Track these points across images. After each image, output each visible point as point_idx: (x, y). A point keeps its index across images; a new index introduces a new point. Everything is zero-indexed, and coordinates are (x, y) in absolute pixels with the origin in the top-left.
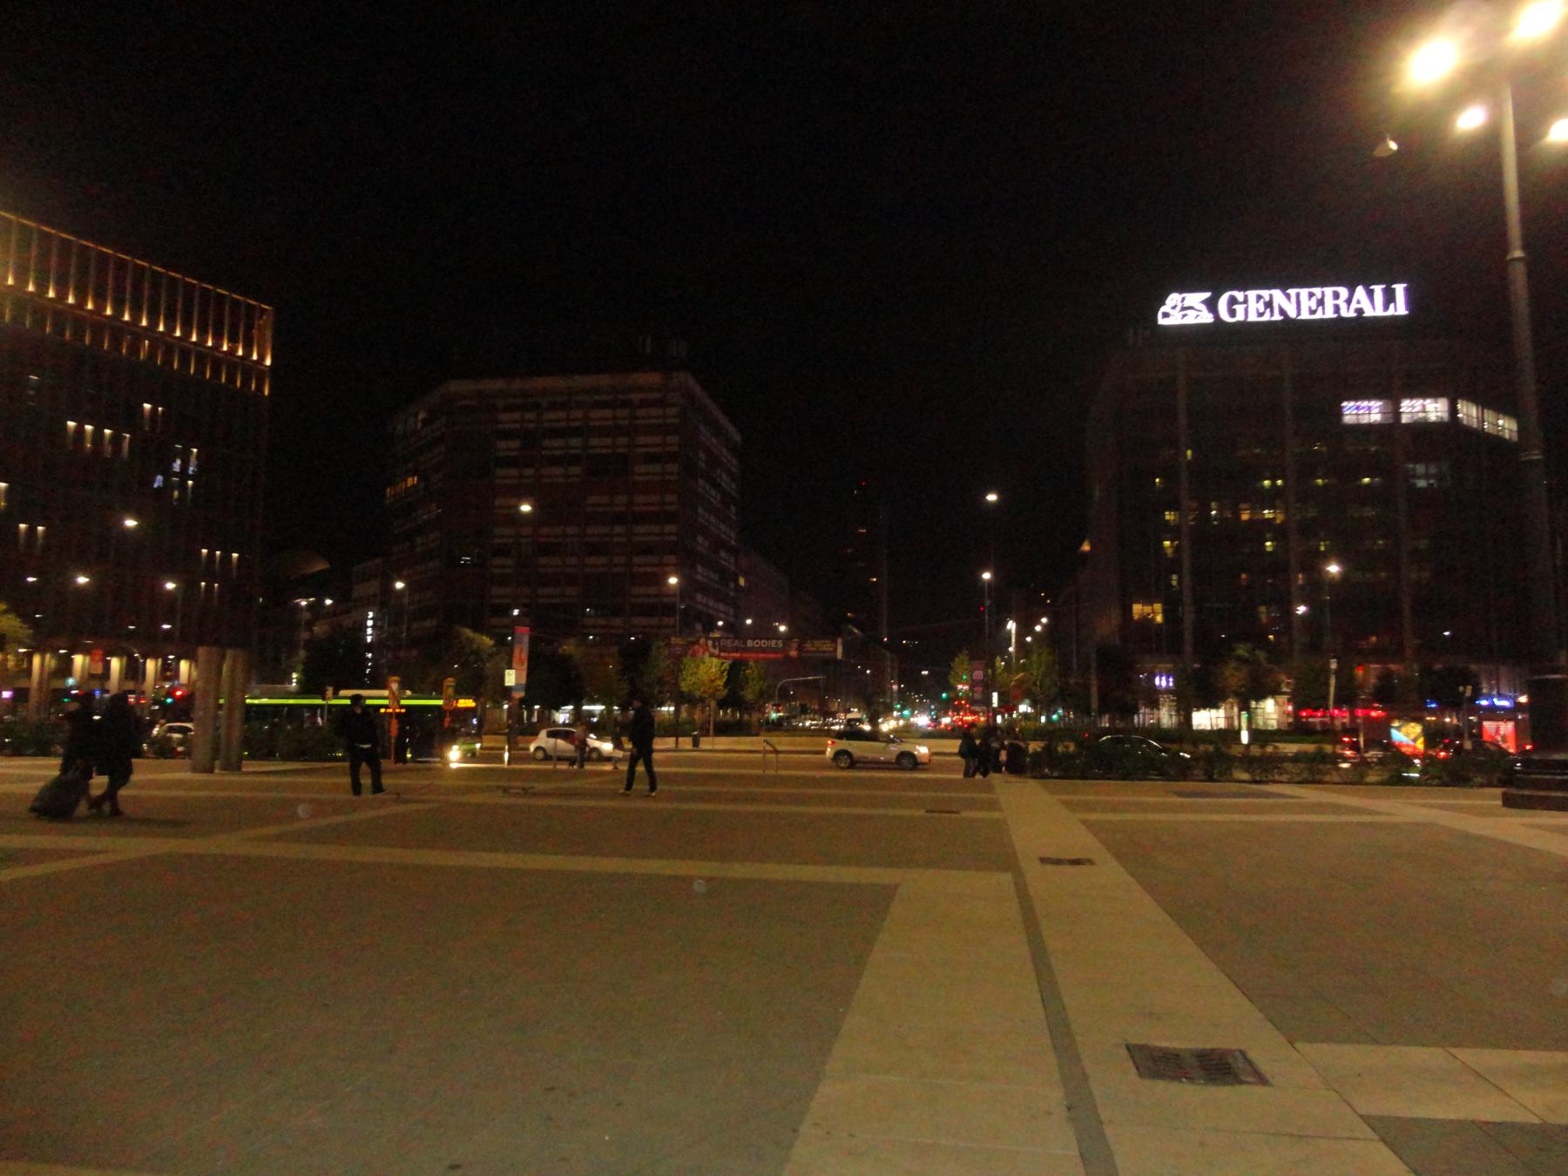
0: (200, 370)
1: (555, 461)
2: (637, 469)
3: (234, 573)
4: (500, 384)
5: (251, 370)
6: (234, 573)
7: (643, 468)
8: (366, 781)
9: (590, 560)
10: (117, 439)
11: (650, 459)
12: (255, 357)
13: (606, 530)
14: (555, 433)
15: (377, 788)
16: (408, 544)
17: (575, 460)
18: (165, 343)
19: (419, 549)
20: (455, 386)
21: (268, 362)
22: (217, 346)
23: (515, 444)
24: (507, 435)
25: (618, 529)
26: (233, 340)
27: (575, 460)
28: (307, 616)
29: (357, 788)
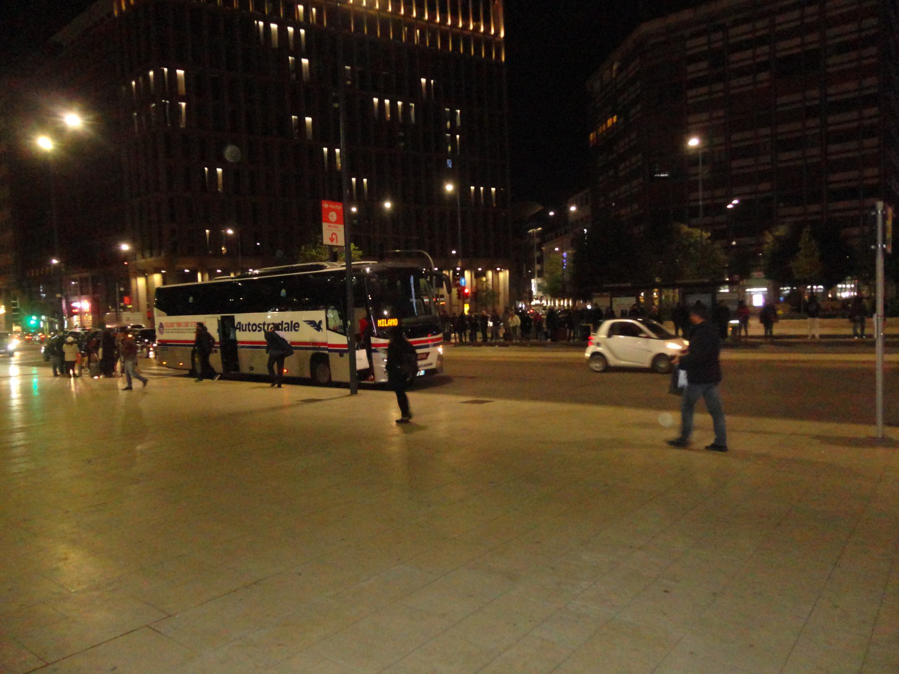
0: (467, 49)
1: (741, 73)
2: (830, 61)
3: (310, 136)
4: (686, 15)
5: (489, 41)
6: (310, 136)
7: (834, 59)
8: (702, 437)
9: (783, 156)
10: (406, 107)
11: (841, 49)
12: (493, 32)
13: (799, 126)
14: (738, 47)
15: (719, 446)
16: (864, 300)
17: (763, 67)
18: (429, 28)
19: (621, 174)
20: (646, 28)
21: (502, 34)
22: (466, 26)
23: (704, 65)
24: (694, 59)
25: (810, 123)
26: (476, 20)
27: (763, 67)
28: (537, 240)
29: (56, 375)
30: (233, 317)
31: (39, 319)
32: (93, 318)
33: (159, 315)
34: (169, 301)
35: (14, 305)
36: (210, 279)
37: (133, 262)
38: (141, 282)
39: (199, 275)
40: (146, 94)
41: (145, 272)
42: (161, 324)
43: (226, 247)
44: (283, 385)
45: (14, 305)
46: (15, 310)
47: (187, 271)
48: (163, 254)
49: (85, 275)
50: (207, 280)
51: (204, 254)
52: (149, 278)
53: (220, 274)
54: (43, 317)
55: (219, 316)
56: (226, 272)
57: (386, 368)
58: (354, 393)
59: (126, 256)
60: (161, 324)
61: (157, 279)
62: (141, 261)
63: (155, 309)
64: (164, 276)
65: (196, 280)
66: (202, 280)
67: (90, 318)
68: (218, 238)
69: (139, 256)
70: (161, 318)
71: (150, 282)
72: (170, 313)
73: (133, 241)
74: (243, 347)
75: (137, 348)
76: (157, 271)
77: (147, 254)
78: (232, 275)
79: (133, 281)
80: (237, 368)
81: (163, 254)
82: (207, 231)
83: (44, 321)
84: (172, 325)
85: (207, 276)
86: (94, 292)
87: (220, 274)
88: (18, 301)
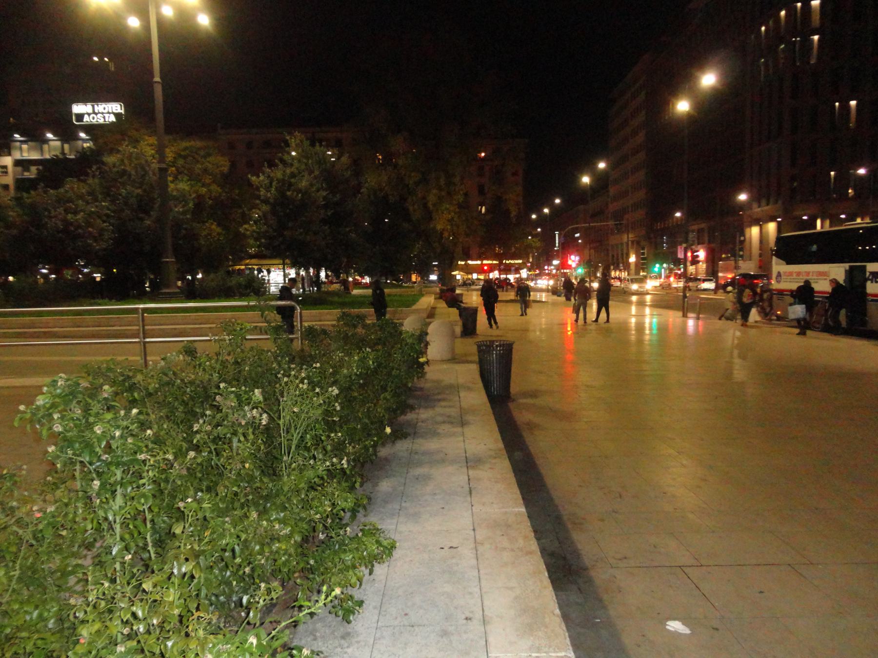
30: (865, 267)
31: (662, 267)
32: (707, 267)
33: (776, 264)
34: (790, 250)
35: (643, 254)
36: (831, 226)
37: (748, 213)
38: (755, 231)
39: (819, 222)
40: (776, 36)
41: (759, 221)
42: (779, 273)
43: (855, 190)
44: (809, 332)
45: (643, 254)
46: (643, 259)
47: (805, 218)
48: (780, 202)
49: (703, 225)
50: (827, 227)
51: (826, 199)
52: (764, 226)
53: (845, 220)
54: (665, 265)
55: (847, 266)
56: (851, 218)
57: (564, 286)
58: (802, 333)
59: (742, 206)
60: (779, 273)
61: (772, 227)
62: (757, 210)
63: (774, 258)
64: (779, 223)
65: (815, 227)
66: (822, 227)
67: (704, 266)
68: (845, 179)
69: (755, 205)
70: (778, 266)
71: (764, 230)
72: (789, 262)
73: (750, 192)
74: (872, 300)
75: (228, 260)
76: (772, 219)
77: (764, 202)
78: (859, 220)
79: (747, 230)
80: (864, 323)
81: (780, 202)
82: (832, 173)
83: (665, 269)
84: (791, 274)
85: (827, 222)
86: (709, 242)
87: (845, 220)
88: (645, 251)
